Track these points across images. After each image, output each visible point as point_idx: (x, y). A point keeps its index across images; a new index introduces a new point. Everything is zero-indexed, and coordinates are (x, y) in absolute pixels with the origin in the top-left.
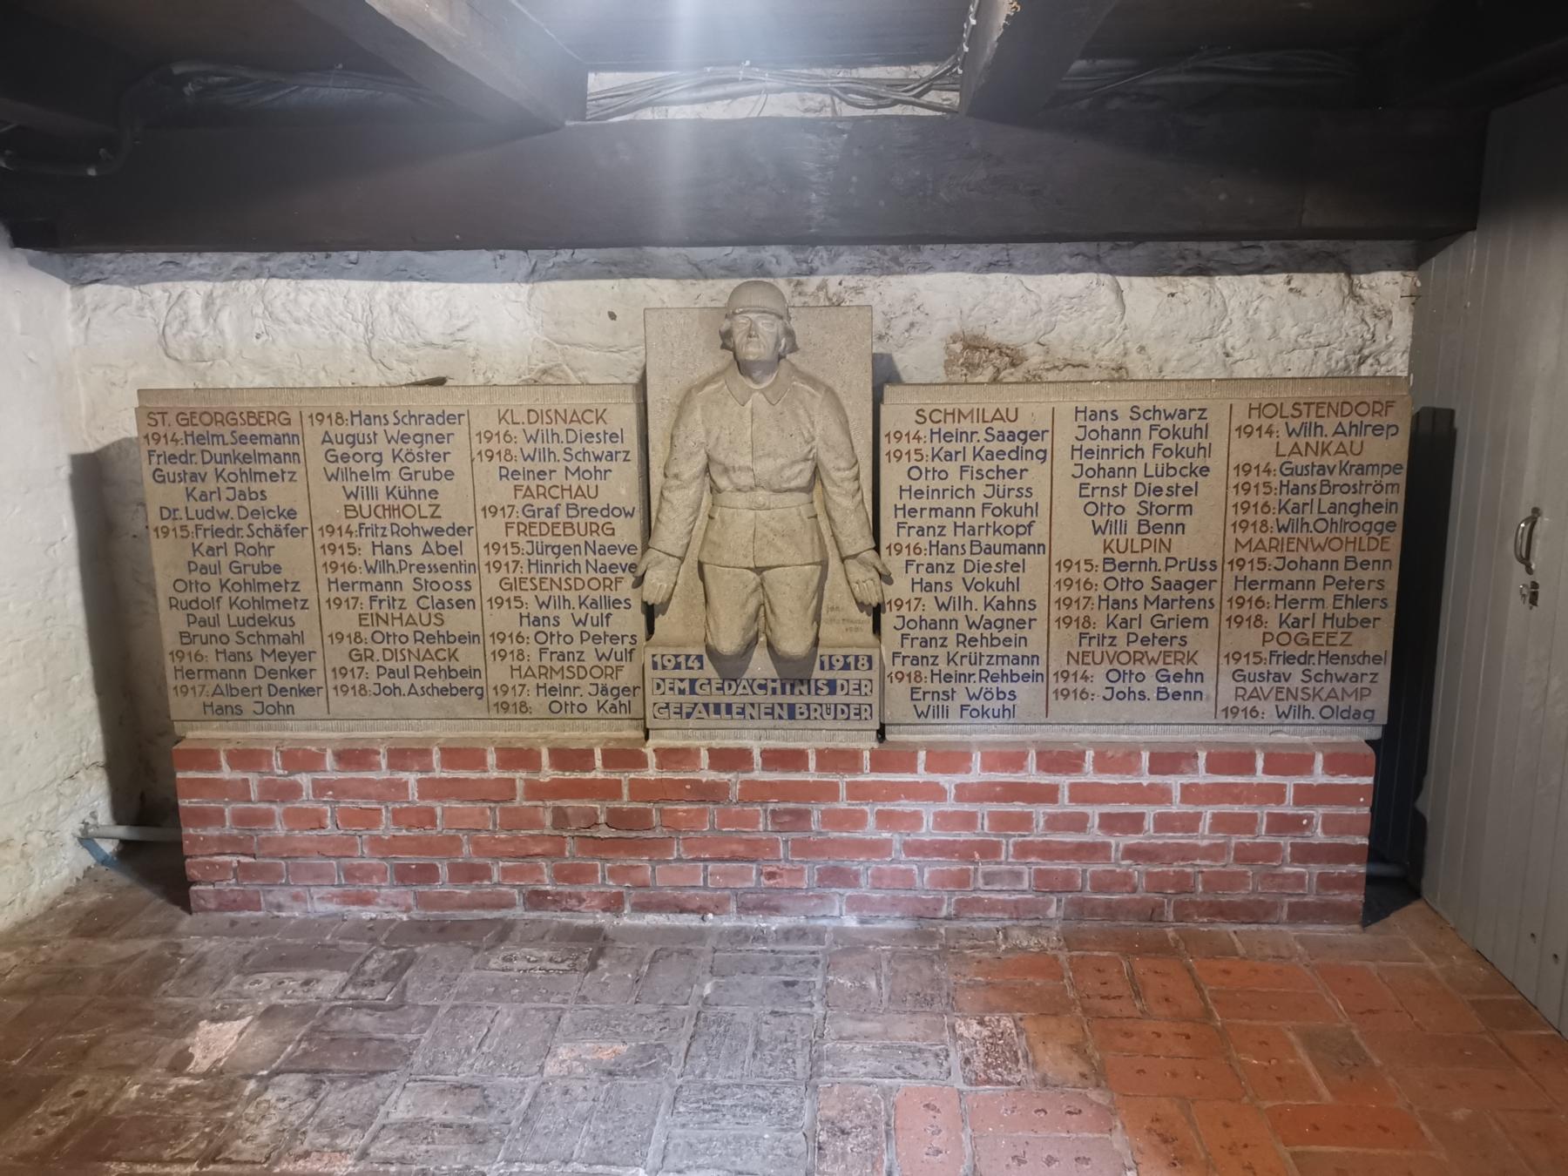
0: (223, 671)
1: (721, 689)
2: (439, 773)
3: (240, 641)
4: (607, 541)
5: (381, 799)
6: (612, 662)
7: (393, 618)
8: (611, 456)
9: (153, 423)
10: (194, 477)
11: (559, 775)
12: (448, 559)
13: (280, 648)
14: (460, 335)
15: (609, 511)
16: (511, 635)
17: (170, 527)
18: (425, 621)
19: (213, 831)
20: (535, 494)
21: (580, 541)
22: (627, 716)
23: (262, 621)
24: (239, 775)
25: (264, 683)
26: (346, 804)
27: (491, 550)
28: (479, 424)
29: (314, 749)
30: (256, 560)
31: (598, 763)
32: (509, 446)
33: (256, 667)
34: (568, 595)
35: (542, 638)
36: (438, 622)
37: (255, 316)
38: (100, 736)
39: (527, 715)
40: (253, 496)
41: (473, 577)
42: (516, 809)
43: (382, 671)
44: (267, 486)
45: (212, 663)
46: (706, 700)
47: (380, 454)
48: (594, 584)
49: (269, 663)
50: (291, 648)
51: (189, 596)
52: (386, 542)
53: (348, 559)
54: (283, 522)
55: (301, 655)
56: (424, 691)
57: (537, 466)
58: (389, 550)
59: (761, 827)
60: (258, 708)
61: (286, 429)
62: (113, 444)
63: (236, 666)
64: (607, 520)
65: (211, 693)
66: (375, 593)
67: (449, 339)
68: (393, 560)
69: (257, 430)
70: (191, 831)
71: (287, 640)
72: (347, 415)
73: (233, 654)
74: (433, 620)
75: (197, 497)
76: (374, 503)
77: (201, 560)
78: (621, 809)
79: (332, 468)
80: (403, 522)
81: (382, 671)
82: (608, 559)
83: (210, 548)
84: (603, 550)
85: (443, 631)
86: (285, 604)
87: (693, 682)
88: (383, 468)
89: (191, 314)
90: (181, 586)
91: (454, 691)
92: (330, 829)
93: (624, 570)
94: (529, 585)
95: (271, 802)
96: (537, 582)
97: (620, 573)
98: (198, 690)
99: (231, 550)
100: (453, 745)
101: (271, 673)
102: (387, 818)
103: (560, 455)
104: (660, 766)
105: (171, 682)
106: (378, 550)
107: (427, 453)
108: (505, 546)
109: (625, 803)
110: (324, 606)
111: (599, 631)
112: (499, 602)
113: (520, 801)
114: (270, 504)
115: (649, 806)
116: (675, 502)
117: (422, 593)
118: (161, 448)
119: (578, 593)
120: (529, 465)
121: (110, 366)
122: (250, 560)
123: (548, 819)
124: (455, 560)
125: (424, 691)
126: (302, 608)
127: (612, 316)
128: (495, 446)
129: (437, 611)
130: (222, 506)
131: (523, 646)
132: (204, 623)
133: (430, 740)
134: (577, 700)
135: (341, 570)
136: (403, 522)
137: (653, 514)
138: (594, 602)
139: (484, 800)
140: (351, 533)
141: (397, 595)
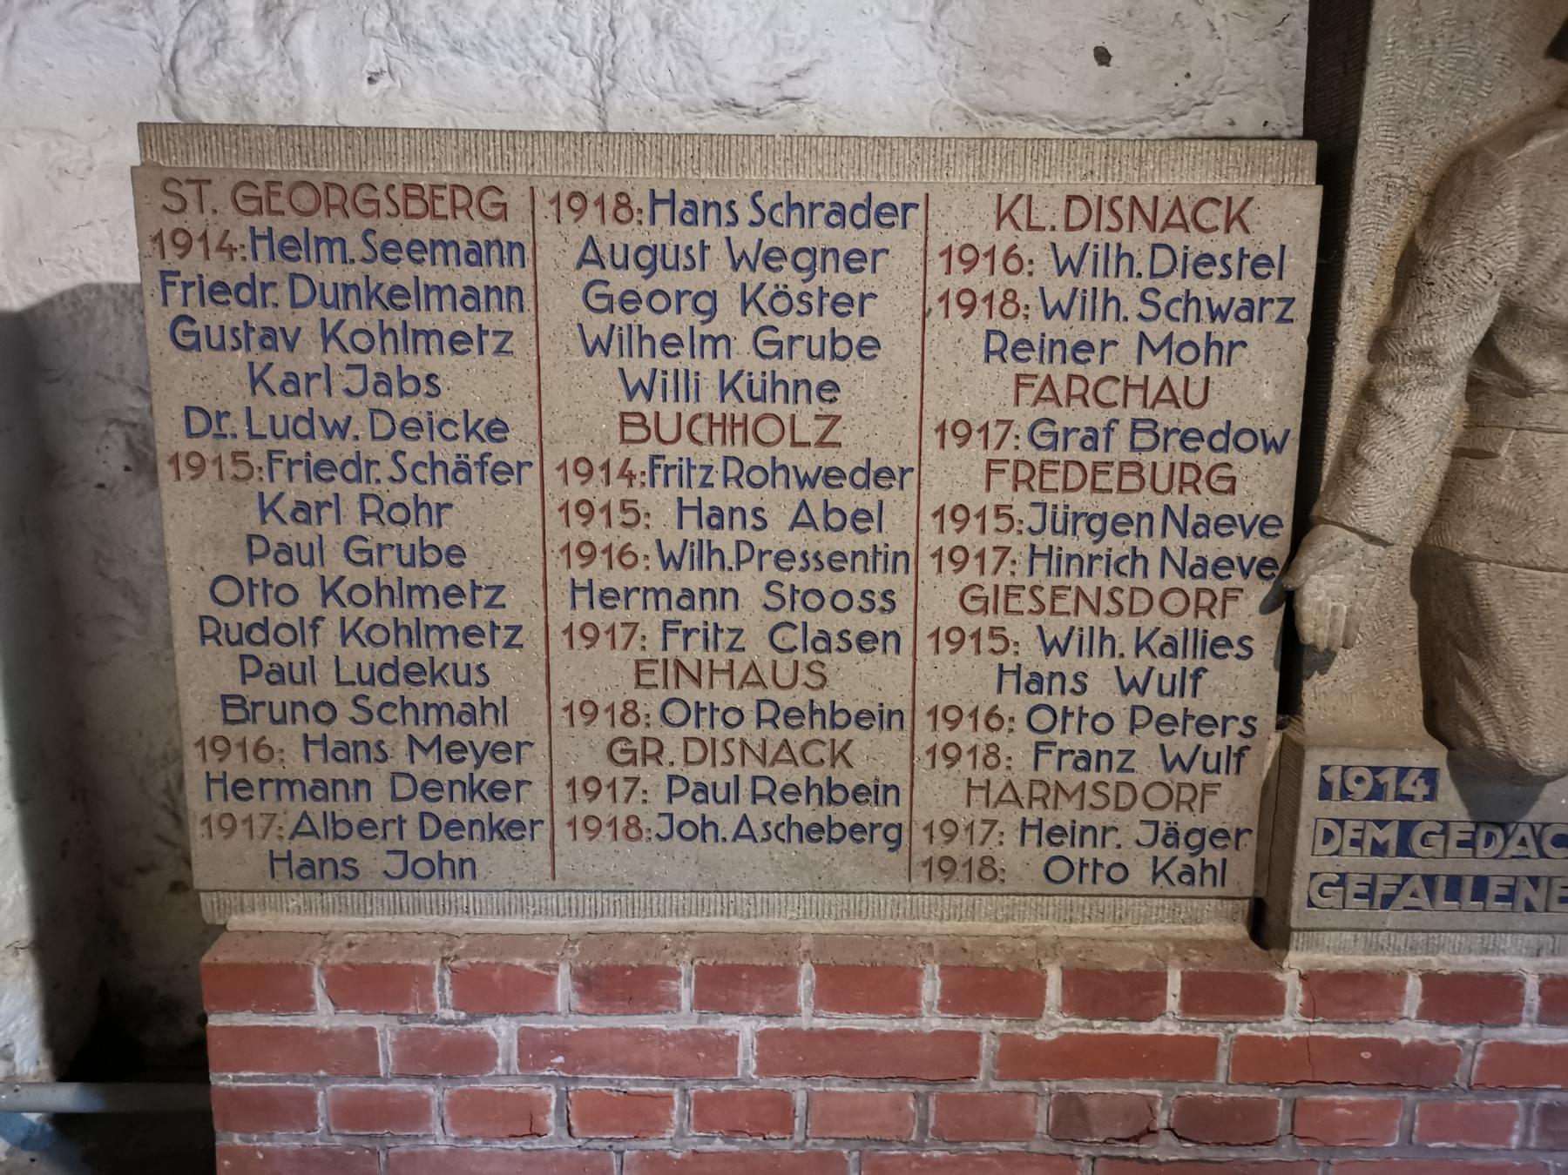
0: (319, 783)
1: (1470, 844)
2: (809, 1018)
3: (363, 716)
4: (1216, 506)
5: (672, 1073)
6: (1197, 775)
7: (712, 671)
8: (1250, 310)
9: (177, 205)
10: (269, 337)
11: (1080, 1026)
12: (848, 541)
13: (451, 733)
14: (791, 88)
15: (1229, 436)
16: (974, 714)
17: (208, 454)
18: (784, 676)
19: (286, 1141)
20: (1062, 395)
21: (1155, 504)
22: (1218, 890)
23: (413, 674)
24: (351, 1021)
25: (411, 810)
26: (596, 1082)
27: (948, 522)
28: (952, 227)
29: (530, 964)
30: (407, 536)
31: (1173, 1003)
32: (1016, 282)
33: (395, 775)
34: (1113, 626)
35: (1043, 719)
36: (814, 681)
37: (368, 34)
38: (22, 888)
39: (995, 887)
40: (409, 386)
41: (900, 582)
42: (975, 1098)
43: (678, 787)
44: (443, 364)
45: (295, 766)
46: (1431, 868)
47: (713, 295)
48: (1174, 603)
49: (426, 767)
50: (478, 735)
51: (246, 615)
52: (710, 498)
53: (618, 537)
54: (474, 449)
55: (497, 750)
56: (771, 830)
57: (1073, 330)
58: (716, 518)
59: (1515, 1140)
60: (396, 865)
61: (497, 230)
62: (61, 296)
63: (348, 772)
64: (1222, 457)
65: (289, 828)
66: (676, 614)
67: (772, 93)
68: (724, 540)
69: (425, 230)
70: (237, 1139)
71: (470, 716)
72: (640, 200)
73: (343, 746)
74: (804, 675)
75: (276, 386)
76: (688, 410)
77: (277, 532)
78: (1207, 1101)
79: (598, 326)
80: (753, 454)
81: (678, 787)
82: (1212, 547)
83: (302, 506)
84: (1206, 526)
85: (822, 701)
86: (470, 635)
87: (1406, 827)
88: (715, 328)
89: (234, 24)
90: (227, 591)
91: (837, 833)
92: (554, 1138)
93: (1246, 574)
94: (1026, 602)
95: (423, 1078)
96: (1045, 596)
97: (1236, 579)
98: (260, 823)
99: (351, 509)
100: (851, 959)
101: (429, 788)
102: (682, 1114)
103: (1131, 306)
104: (1311, 1011)
105: (196, 802)
106: (690, 517)
107: (823, 294)
108: (982, 514)
109: (1221, 1087)
110: (559, 642)
111: (1175, 706)
112: (954, 639)
113: (986, 1082)
114: (444, 406)
115: (1271, 1094)
116: (1409, 416)
117: (783, 615)
118: (193, 265)
119: (1136, 621)
120: (1057, 328)
121: (58, 132)
122: (394, 534)
123: (1041, 1120)
124: (863, 543)
125: (771, 830)
126: (508, 645)
127: (1102, 56)
128: (980, 279)
129: (811, 656)
130: (334, 408)
131: (999, 737)
132: (279, 674)
133: (782, 942)
134: (1107, 857)
135: (601, 561)
136: (753, 454)
137: (1331, 446)
138: (1171, 642)
139: (906, 1079)
140: (631, 477)
141: (727, 619)
